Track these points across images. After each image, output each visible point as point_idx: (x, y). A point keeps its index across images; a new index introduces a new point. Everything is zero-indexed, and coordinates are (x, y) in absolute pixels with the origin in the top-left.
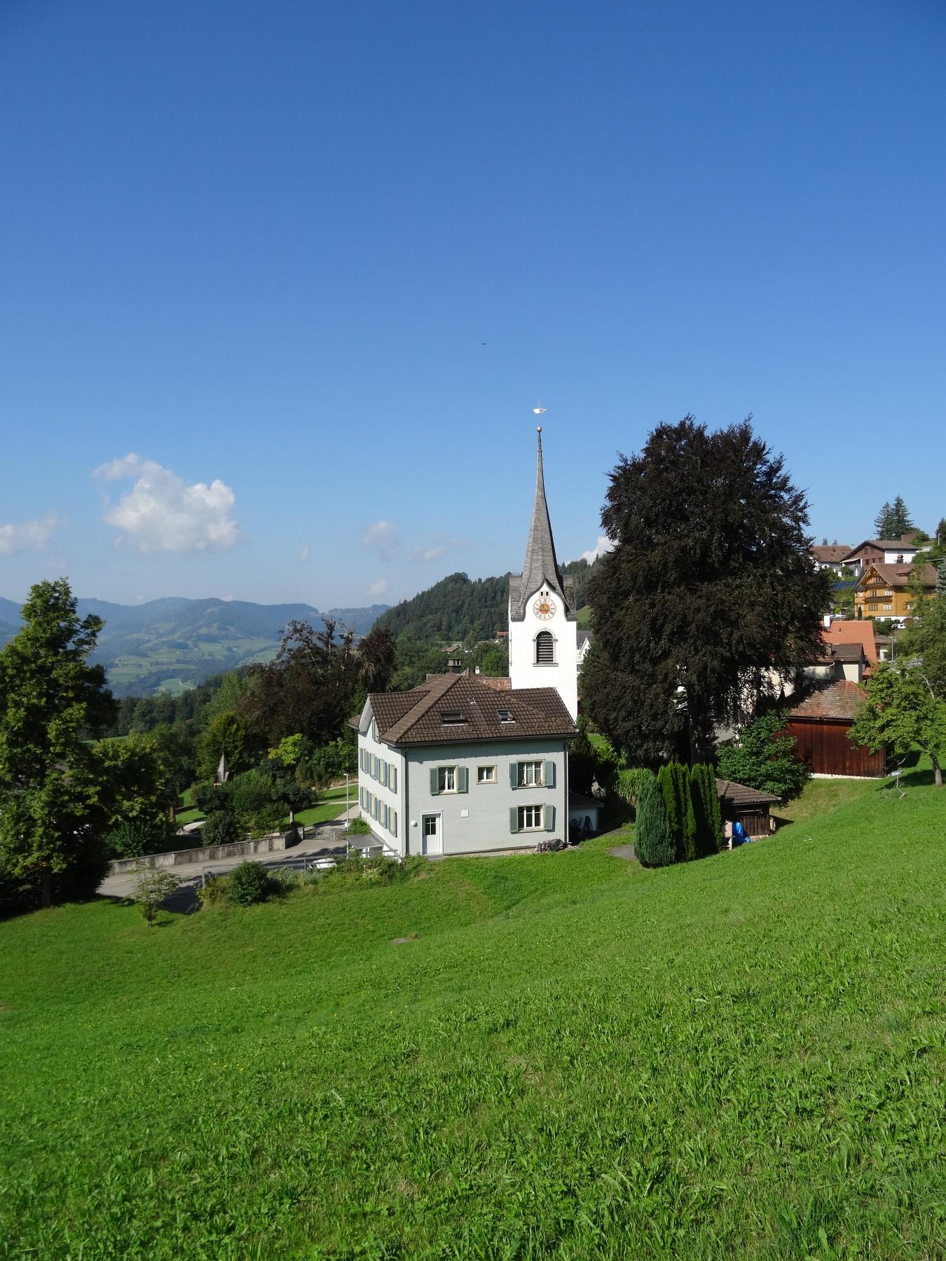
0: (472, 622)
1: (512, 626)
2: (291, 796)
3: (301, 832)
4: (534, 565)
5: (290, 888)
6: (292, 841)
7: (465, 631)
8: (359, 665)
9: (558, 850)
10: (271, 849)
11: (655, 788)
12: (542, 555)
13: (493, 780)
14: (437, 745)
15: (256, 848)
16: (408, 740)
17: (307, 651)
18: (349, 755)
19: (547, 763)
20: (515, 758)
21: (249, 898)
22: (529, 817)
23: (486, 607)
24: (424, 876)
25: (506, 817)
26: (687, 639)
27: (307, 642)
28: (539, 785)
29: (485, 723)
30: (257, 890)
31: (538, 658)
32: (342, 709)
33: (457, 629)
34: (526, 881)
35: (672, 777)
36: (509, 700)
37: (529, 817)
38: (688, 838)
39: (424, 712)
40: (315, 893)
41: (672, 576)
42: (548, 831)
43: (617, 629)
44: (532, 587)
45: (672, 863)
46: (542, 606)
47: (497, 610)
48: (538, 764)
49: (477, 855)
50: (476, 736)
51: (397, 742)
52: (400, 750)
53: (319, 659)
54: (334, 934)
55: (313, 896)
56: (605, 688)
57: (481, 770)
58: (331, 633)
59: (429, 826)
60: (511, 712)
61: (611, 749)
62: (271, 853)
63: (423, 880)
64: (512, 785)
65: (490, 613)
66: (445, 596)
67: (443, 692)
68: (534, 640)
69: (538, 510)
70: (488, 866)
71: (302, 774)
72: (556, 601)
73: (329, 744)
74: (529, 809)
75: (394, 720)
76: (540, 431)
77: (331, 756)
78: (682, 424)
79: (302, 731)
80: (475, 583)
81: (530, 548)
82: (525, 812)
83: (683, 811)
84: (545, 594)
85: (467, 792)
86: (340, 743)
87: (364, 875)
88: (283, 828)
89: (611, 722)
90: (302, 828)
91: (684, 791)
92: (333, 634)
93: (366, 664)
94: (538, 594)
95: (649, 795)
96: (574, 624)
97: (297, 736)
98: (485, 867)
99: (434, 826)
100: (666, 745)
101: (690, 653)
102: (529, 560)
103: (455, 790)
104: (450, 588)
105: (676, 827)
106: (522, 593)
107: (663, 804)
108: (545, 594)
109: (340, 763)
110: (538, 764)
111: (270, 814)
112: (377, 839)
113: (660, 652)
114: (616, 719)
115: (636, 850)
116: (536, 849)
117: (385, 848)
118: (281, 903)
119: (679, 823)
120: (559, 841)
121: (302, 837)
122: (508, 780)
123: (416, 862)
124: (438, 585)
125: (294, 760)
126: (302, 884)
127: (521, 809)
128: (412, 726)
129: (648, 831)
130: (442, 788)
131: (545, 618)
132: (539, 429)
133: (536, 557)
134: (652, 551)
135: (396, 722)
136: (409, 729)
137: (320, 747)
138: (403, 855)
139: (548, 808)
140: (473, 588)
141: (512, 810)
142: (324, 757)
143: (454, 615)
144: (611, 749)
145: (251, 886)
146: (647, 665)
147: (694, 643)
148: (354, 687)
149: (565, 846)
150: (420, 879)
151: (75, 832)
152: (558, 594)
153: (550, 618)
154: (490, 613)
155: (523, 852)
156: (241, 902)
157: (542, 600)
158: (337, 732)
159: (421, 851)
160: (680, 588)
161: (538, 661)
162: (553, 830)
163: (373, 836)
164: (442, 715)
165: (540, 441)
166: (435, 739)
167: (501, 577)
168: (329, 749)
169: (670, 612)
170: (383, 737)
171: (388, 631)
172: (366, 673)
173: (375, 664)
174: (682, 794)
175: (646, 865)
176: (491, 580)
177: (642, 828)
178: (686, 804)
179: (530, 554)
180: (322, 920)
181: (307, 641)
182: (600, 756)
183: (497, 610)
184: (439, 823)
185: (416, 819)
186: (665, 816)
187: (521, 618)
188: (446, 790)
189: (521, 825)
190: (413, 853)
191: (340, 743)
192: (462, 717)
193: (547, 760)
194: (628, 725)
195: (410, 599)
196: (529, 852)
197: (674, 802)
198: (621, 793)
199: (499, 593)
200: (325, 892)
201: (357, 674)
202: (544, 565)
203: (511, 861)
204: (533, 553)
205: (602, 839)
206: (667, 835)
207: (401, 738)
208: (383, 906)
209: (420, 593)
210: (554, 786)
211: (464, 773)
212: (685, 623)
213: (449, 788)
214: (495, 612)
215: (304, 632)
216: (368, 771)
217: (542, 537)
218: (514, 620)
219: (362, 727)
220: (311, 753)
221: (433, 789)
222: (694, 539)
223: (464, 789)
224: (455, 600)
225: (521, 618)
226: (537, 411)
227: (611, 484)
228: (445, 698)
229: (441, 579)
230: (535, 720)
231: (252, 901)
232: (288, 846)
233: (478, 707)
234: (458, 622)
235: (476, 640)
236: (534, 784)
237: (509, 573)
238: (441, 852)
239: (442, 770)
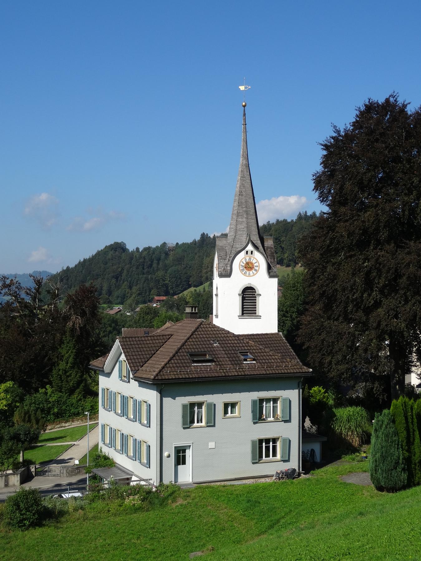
0: (130, 288)
1: (217, 281)
2: (21, 436)
3: (33, 470)
4: (239, 227)
5: (62, 513)
6: (26, 478)
7: (124, 295)
8: (66, 318)
9: (293, 479)
10: (7, 485)
11: (390, 420)
12: (247, 218)
13: (237, 414)
14: (181, 383)
16: (164, 378)
17: (16, 305)
18: (58, 401)
19: (284, 400)
20: (256, 395)
21: (27, 523)
22: (267, 448)
23: (144, 274)
24: (180, 501)
25: (248, 449)
26: (398, 290)
27: (15, 297)
28: (277, 420)
29: (229, 363)
30: (34, 515)
31: (243, 311)
32: (50, 359)
33: (116, 293)
34: (277, 504)
35: (403, 410)
36: (248, 343)
37: (267, 448)
38: (415, 464)
39: (174, 352)
40: (85, 519)
41: (384, 235)
42: (284, 461)
43: (333, 282)
44: (237, 246)
45: (404, 487)
46: (247, 263)
47: (154, 277)
48: (275, 400)
49: (223, 483)
50: (224, 375)
51: (154, 379)
52: (155, 387)
53: (27, 312)
54: (117, 552)
55: (84, 520)
56: (320, 335)
57: (226, 405)
58: (39, 288)
59: (180, 458)
60: (251, 353)
61: (323, 391)
63: (181, 505)
64: (253, 419)
65: (147, 279)
66: (106, 263)
67: (188, 335)
68: (239, 295)
69: (243, 177)
70: (237, 492)
71: (21, 417)
72: (260, 260)
73: (38, 391)
74: (267, 441)
75: (143, 360)
76: (244, 106)
77: (41, 402)
78: (387, 100)
79: (12, 380)
80: (133, 252)
81: (235, 212)
82: (264, 444)
83: (412, 440)
84: (249, 253)
85: (214, 426)
86: (49, 390)
87: (127, 501)
88: (16, 466)
89: (326, 366)
90: (33, 466)
91: (412, 422)
92: (40, 290)
93: (73, 317)
94: (243, 253)
95: (384, 426)
96: (275, 281)
97: (9, 384)
98: (235, 493)
99: (184, 457)
100: (376, 386)
101: (400, 303)
102: (234, 223)
103: (203, 424)
104: (109, 256)
105: (407, 454)
106: (229, 253)
107: (396, 433)
108: (249, 253)
109: (50, 409)
110: (275, 400)
111: (5, 453)
112: (123, 470)
113: (372, 302)
114: (330, 363)
115: (372, 475)
116: (274, 478)
117: (134, 478)
118: (58, 528)
119: (409, 451)
120: (294, 470)
121: (34, 474)
122: (250, 415)
123: (170, 491)
124: (99, 253)
125: (6, 406)
126: (71, 510)
127: (261, 441)
128: (166, 365)
129: (384, 458)
130: (192, 422)
131: (249, 274)
132: (244, 104)
133: (240, 220)
134: (364, 212)
135: (146, 362)
136: (163, 368)
137: (30, 394)
138: (156, 484)
139: (284, 440)
140: (132, 256)
141: (253, 442)
142: (34, 403)
143: (114, 281)
144: (323, 391)
145: (29, 511)
146: (360, 313)
147: (405, 293)
148: (61, 339)
149: (299, 475)
150: (178, 504)
152: (261, 253)
153: (254, 275)
154: (147, 279)
155: (263, 480)
156: (19, 527)
157: (248, 258)
158: (45, 380)
159: (173, 480)
160: (390, 245)
161: (243, 314)
162: (288, 461)
163: (117, 467)
164: (191, 355)
165: (245, 115)
166: (187, 376)
167: (157, 247)
168: (39, 396)
169: (384, 266)
170: (135, 375)
171: (93, 287)
172: (73, 326)
173: (82, 317)
174: (411, 426)
175: (380, 489)
176: (148, 249)
177: (378, 455)
178: (414, 435)
179: (235, 217)
180: (100, 542)
181: (16, 295)
182: (312, 396)
183: (154, 277)
184: (189, 454)
185: (170, 451)
186: (398, 445)
187: (226, 274)
188: (196, 424)
189: (261, 456)
190: (166, 482)
191: (49, 390)
192: (208, 357)
193: (284, 397)
194: (342, 367)
195: (72, 265)
196: (268, 480)
197: (405, 433)
198: (337, 429)
199: (155, 261)
200: (94, 518)
201: (65, 326)
202: (248, 227)
203: (256, 488)
204: (238, 216)
205: (329, 468)
206: (401, 461)
207: (157, 375)
208: (154, 528)
209: (82, 260)
210: (289, 421)
211: (212, 408)
212: (398, 276)
213: (198, 422)
214: (152, 279)
215: (13, 288)
216: (110, 408)
217: (246, 202)
218: (221, 276)
219: (107, 369)
220: (22, 400)
221: (184, 423)
222: (403, 202)
223: (211, 423)
224: (115, 267)
225: (226, 274)
226: (242, 88)
227: (325, 153)
228: (190, 340)
229: (101, 247)
230: (273, 361)
231: (29, 526)
232: (23, 481)
233: (221, 349)
234: (118, 287)
235: (137, 303)
236: (272, 419)
237: (165, 243)
238: (191, 481)
239: (192, 405)
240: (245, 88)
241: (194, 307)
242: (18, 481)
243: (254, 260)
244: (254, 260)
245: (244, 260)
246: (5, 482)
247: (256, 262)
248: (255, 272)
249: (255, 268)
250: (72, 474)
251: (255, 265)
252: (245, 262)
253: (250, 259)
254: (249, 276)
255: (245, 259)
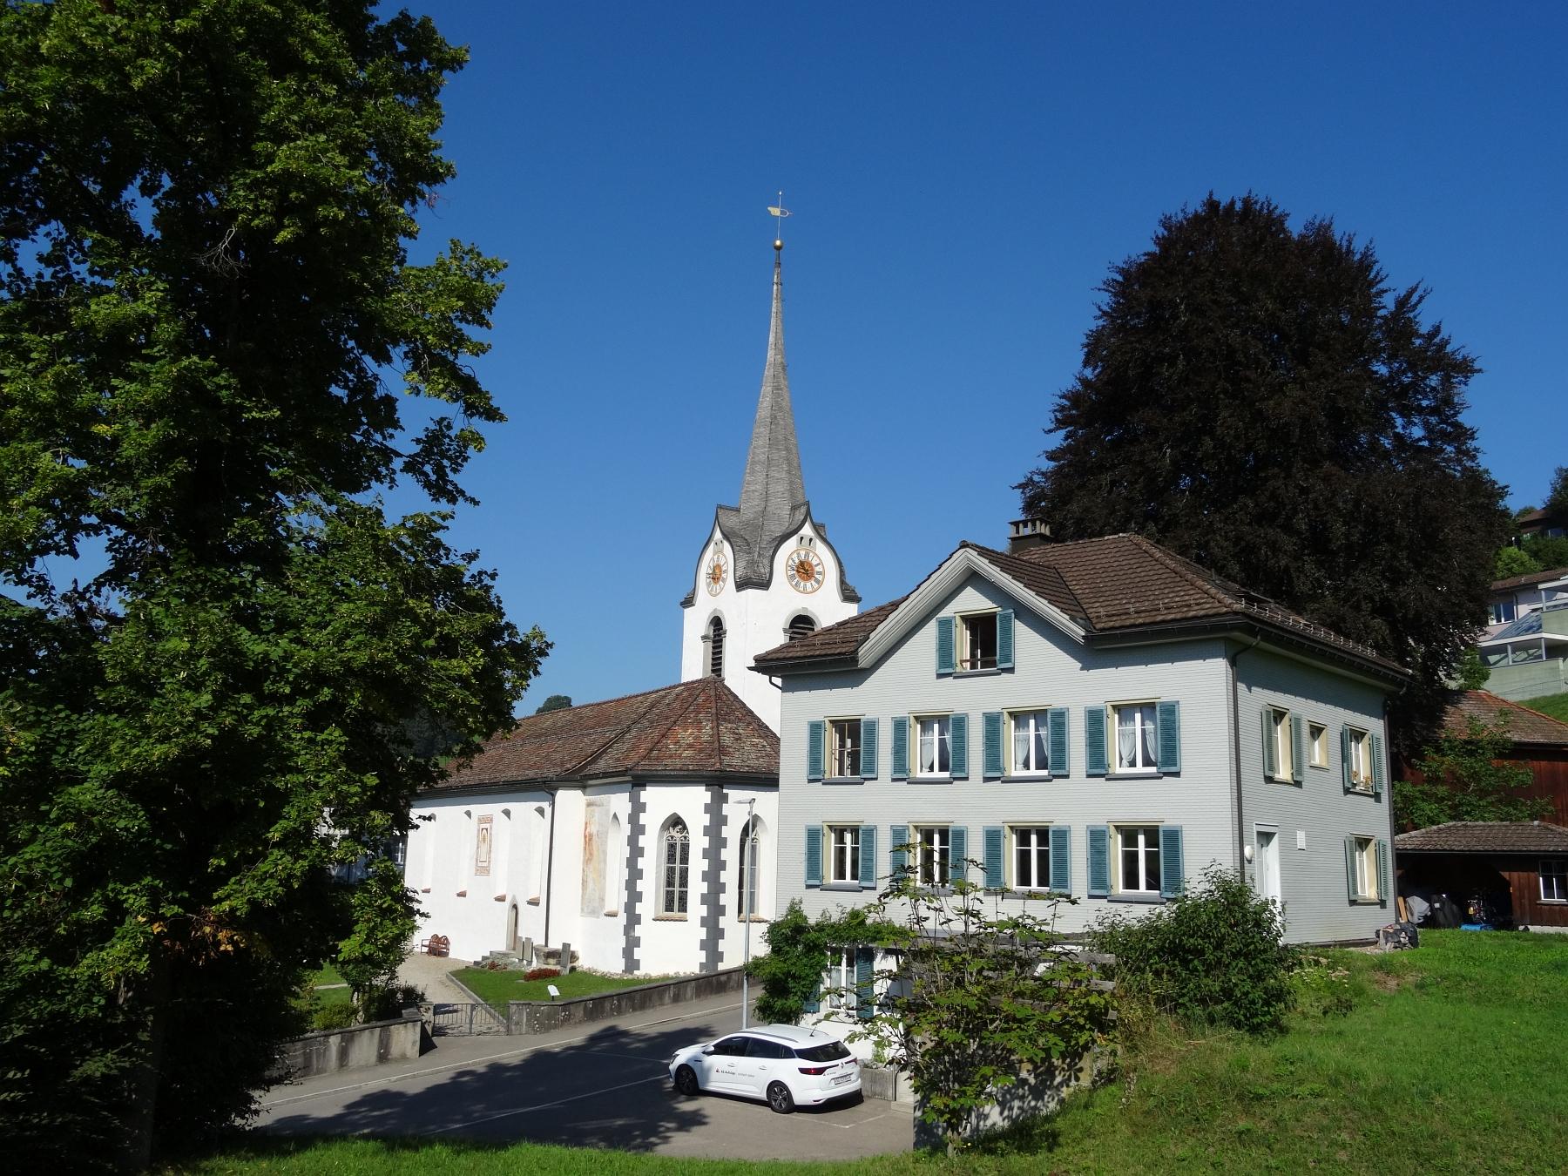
12: (789, 472)
15: (343, 1054)
46: (802, 564)
62: (383, 1069)
80: (1302, 236)
84: (806, 541)
94: (794, 540)
108: (806, 541)
151: (12, 184)
157: (803, 553)
240: (782, 212)
241: (1020, 522)
242: (414, 1042)
243: (815, 558)
244: (815, 558)
245: (795, 555)
246: (380, 1047)
247: (818, 564)
248: (816, 586)
249: (817, 576)
250: (549, 1024)
251: (817, 569)
252: (797, 561)
253: (807, 555)
254: (805, 592)
255: (799, 555)
